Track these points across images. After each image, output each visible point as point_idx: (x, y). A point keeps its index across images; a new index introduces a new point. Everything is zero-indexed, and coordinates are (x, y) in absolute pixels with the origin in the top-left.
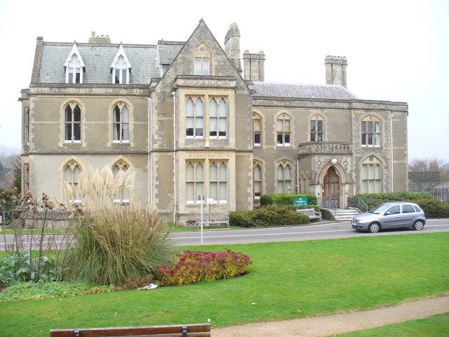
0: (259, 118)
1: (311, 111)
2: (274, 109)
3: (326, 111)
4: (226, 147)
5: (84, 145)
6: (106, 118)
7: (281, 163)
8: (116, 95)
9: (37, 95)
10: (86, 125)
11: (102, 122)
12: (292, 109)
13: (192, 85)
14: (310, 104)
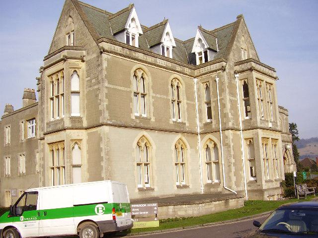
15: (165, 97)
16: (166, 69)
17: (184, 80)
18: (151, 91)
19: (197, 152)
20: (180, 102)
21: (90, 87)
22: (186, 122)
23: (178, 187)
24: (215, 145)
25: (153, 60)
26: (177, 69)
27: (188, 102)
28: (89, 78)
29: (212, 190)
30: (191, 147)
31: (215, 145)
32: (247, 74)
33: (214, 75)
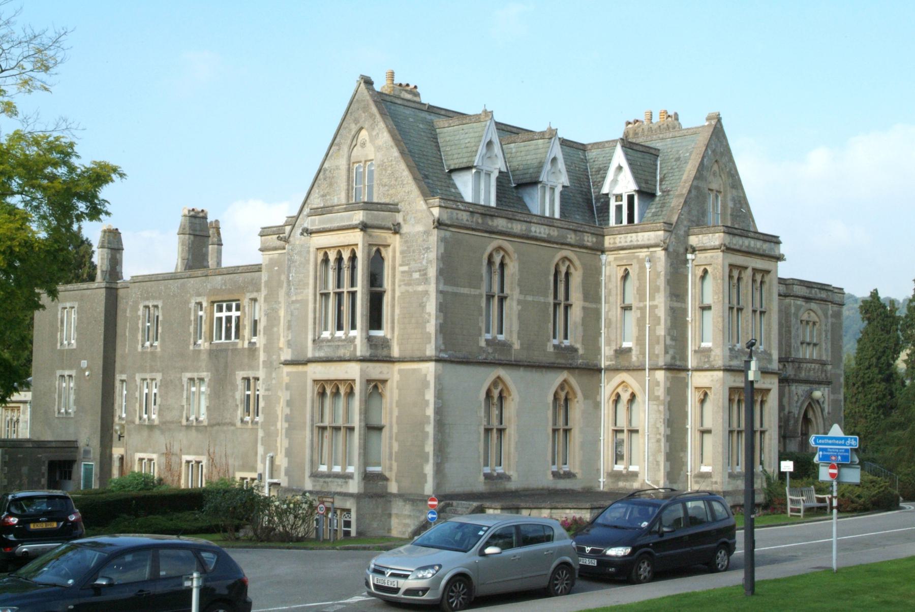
8: (562, 244)
13: (623, 244)
15: (542, 299)
16: (549, 242)
17: (579, 259)
18: (517, 290)
19: (597, 405)
20: (571, 305)
21: (409, 284)
22: (578, 346)
23: (556, 475)
24: (633, 396)
25: (524, 228)
26: (569, 240)
27: (587, 305)
28: (406, 268)
29: (621, 484)
30: (586, 397)
31: (633, 396)
32: (712, 257)
33: (643, 253)
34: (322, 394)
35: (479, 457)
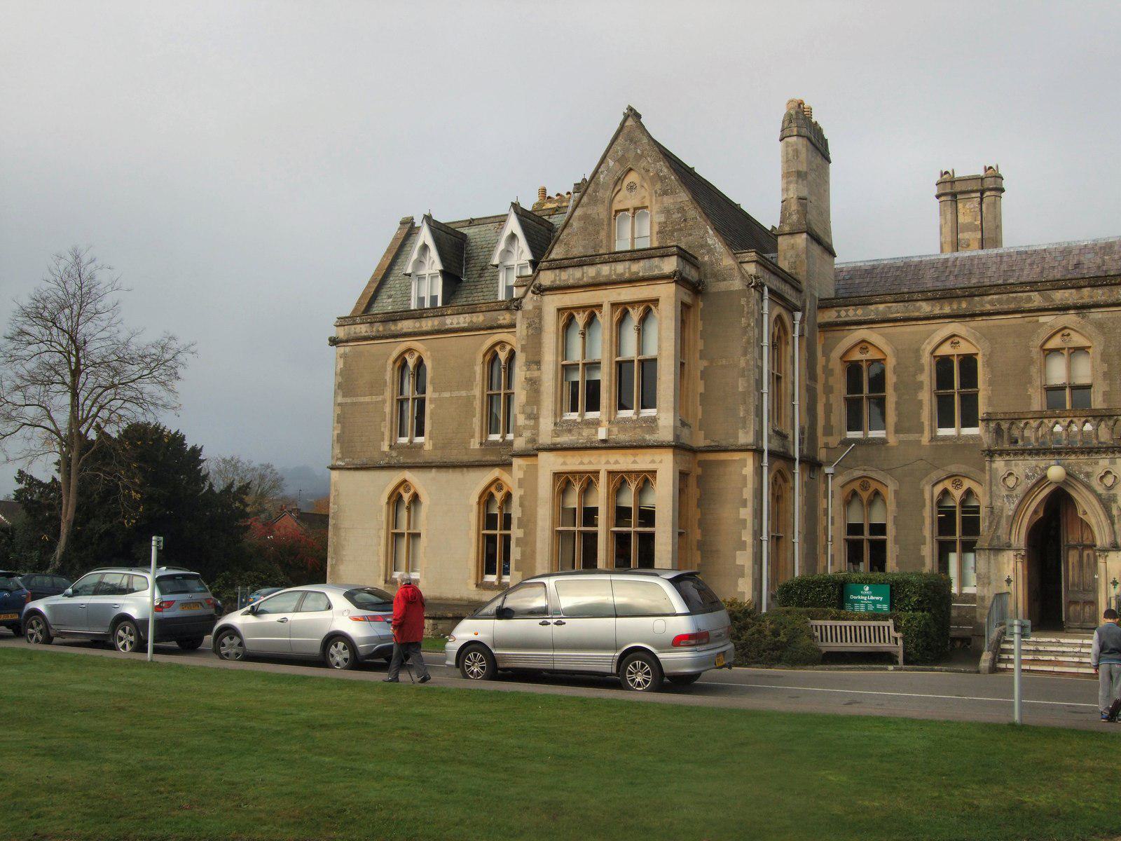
0: (878, 356)
1: (1042, 320)
2: (921, 327)
3: (1096, 315)
4: (649, 438)
5: (428, 447)
6: (469, 384)
7: (948, 484)
8: (491, 328)
9: (347, 341)
10: (431, 401)
11: (464, 393)
12: (979, 323)
13: (571, 282)
14: (1037, 300)
34: (570, 320)
35: (378, 561)
